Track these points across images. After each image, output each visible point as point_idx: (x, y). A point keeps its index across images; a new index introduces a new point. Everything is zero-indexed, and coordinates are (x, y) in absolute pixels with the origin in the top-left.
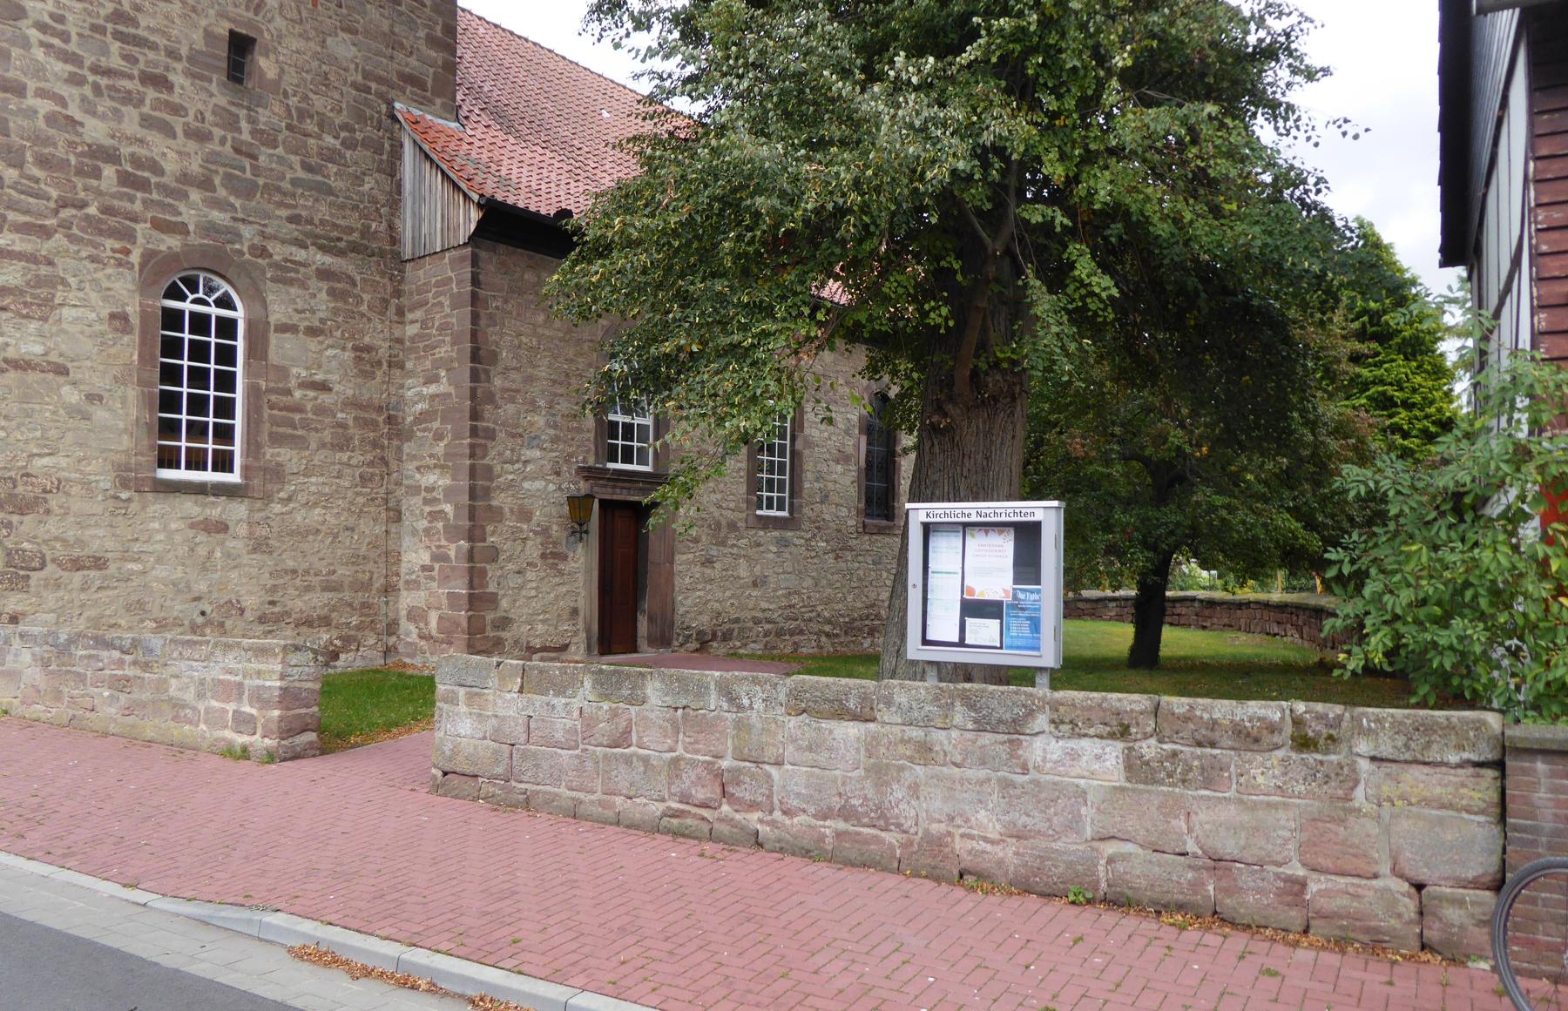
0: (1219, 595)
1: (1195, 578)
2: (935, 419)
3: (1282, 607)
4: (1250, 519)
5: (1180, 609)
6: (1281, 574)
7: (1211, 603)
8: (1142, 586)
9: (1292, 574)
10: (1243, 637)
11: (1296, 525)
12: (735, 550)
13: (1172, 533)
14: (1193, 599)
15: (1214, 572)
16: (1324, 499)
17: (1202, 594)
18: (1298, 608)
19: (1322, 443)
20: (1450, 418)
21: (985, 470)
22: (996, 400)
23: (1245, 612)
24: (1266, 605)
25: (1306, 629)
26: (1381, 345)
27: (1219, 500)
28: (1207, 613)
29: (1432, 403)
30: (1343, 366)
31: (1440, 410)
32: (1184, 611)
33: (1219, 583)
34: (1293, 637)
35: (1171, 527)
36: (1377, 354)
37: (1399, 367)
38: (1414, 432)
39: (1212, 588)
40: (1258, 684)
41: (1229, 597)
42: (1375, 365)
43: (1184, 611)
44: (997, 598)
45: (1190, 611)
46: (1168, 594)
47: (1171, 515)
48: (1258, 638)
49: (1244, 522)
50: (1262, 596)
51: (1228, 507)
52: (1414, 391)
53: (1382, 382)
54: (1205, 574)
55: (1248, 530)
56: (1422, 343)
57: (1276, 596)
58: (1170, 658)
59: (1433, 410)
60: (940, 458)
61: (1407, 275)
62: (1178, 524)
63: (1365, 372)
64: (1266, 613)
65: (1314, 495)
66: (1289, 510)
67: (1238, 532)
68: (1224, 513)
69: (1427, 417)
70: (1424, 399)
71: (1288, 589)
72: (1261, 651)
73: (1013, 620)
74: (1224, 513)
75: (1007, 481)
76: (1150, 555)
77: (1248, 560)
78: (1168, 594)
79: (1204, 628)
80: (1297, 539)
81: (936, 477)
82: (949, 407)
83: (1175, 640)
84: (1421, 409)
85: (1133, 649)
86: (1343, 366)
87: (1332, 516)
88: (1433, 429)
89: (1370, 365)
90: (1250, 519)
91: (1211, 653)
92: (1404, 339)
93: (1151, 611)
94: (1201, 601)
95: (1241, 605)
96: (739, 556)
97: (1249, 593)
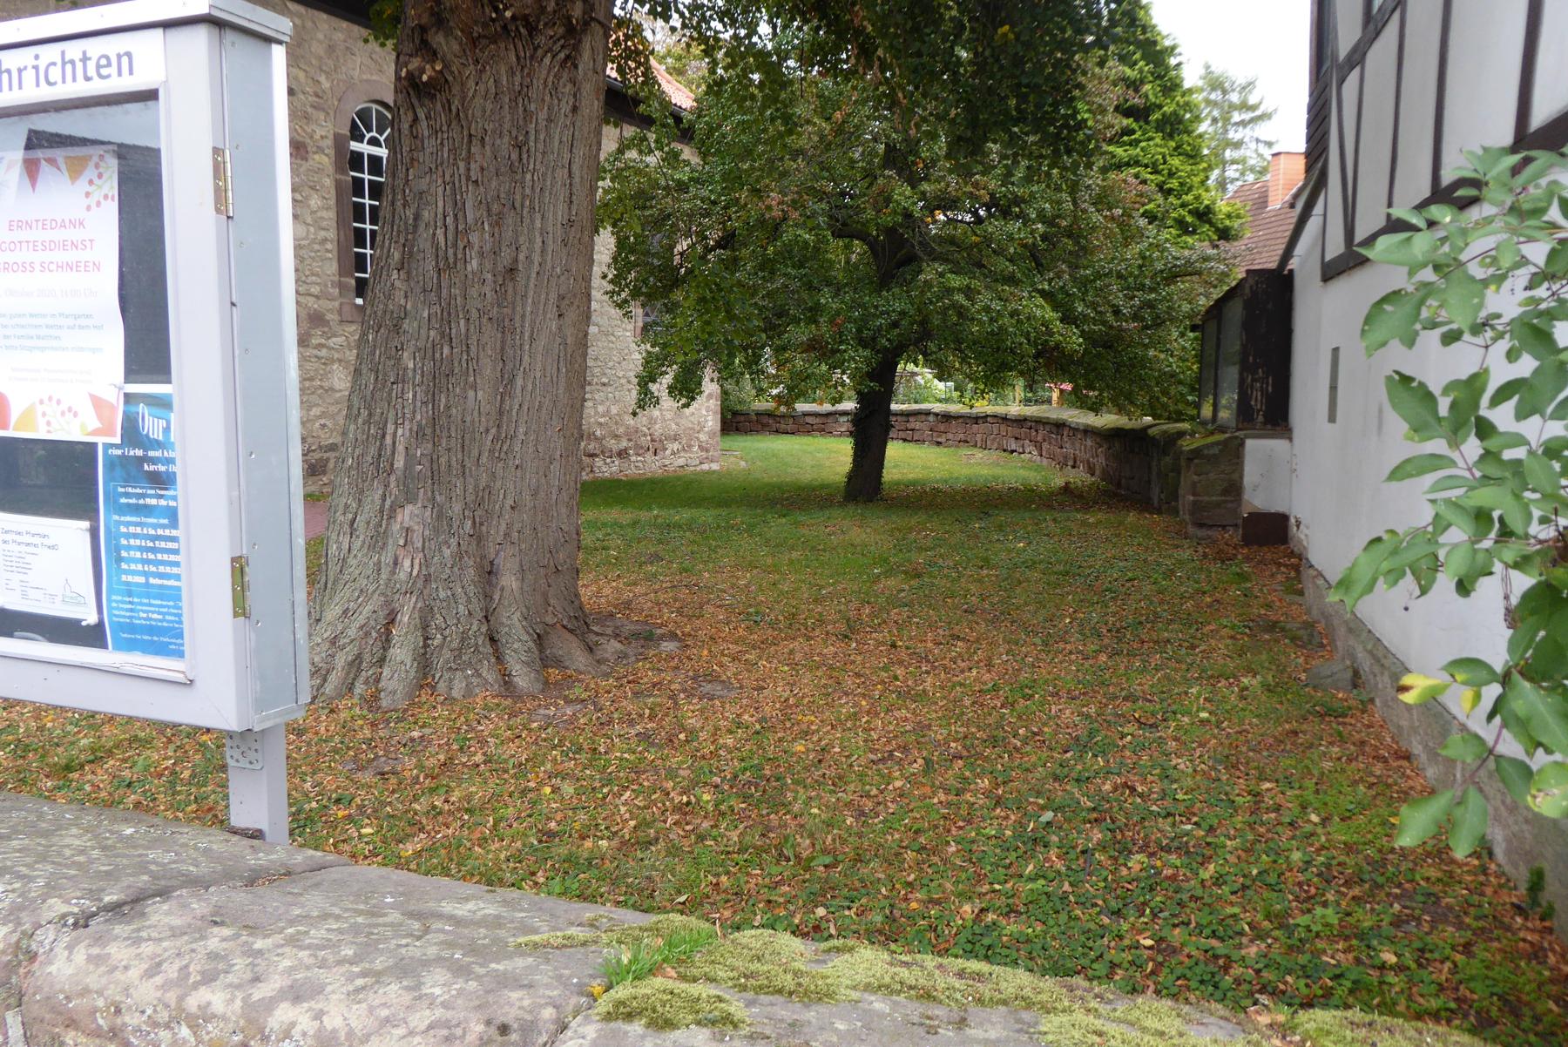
0: (955, 408)
1: (925, 387)
2: (415, 63)
3: (1021, 421)
4: (996, 306)
5: (914, 423)
6: (1020, 384)
7: (947, 417)
8: (862, 398)
9: (1030, 387)
10: (979, 454)
11: (1050, 314)
12: (324, 352)
13: (895, 325)
14: (928, 413)
15: (950, 384)
16: (1084, 284)
17: (938, 407)
18: (1039, 422)
19: (1084, 211)
20: (1207, 207)
21: (515, 170)
22: (532, 30)
23: (982, 427)
24: (1004, 419)
25: (1045, 446)
26: (1136, 120)
27: (956, 281)
28: (942, 427)
29: (1190, 189)
30: (1109, 118)
31: (1197, 198)
32: (918, 425)
33: (956, 394)
34: (1031, 454)
35: (894, 316)
36: (1133, 132)
37: (1157, 146)
38: (1169, 223)
39: (947, 400)
40: (1000, 528)
41: (966, 410)
42: (1130, 144)
43: (918, 425)
44: (71, 431)
45: (925, 426)
46: (894, 407)
47: (895, 302)
48: (995, 455)
49: (987, 309)
50: (1000, 409)
51: (969, 292)
52: (1171, 175)
53: (1137, 163)
54: (941, 385)
55: (992, 320)
56: (1180, 121)
57: (1015, 409)
58: (898, 483)
59: (1189, 198)
60: (430, 145)
61: (1167, 43)
62: (903, 313)
63: (1119, 151)
64: (1003, 427)
65: (1074, 279)
66: (1043, 293)
67: (980, 322)
68: (960, 298)
69: (1183, 206)
70: (1181, 184)
71: (1027, 401)
72: (998, 471)
73: (129, 525)
74: (960, 298)
75: (563, 194)
76: (867, 353)
77: (994, 361)
78: (894, 407)
79: (939, 443)
80: (1050, 333)
81: (423, 184)
82: (438, 40)
83: (904, 460)
84: (1179, 197)
85: (851, 476)
86: (1109, 118)
87: (1094, 306)
88: (1189, 219)
89: (1124, 144)
90: (996, 306)
91: (946, 475)
92: (1164, 115)
93: (872, 427)
94: (937, 415)
95: (977, 419)
96: (333, 361)
97: (983, 407)
